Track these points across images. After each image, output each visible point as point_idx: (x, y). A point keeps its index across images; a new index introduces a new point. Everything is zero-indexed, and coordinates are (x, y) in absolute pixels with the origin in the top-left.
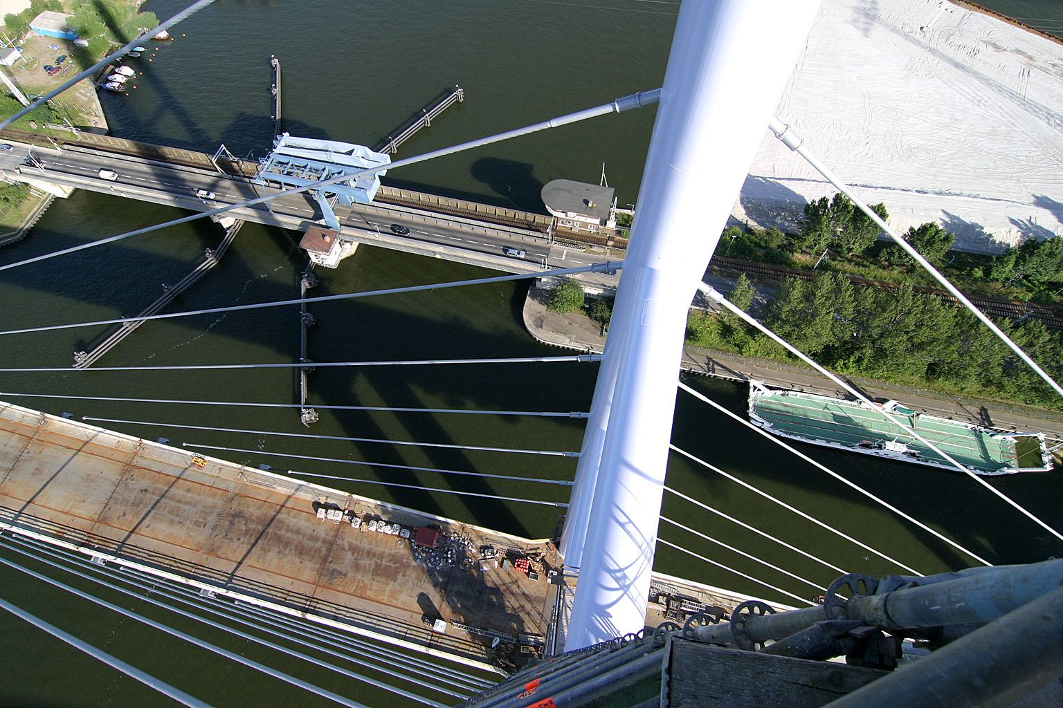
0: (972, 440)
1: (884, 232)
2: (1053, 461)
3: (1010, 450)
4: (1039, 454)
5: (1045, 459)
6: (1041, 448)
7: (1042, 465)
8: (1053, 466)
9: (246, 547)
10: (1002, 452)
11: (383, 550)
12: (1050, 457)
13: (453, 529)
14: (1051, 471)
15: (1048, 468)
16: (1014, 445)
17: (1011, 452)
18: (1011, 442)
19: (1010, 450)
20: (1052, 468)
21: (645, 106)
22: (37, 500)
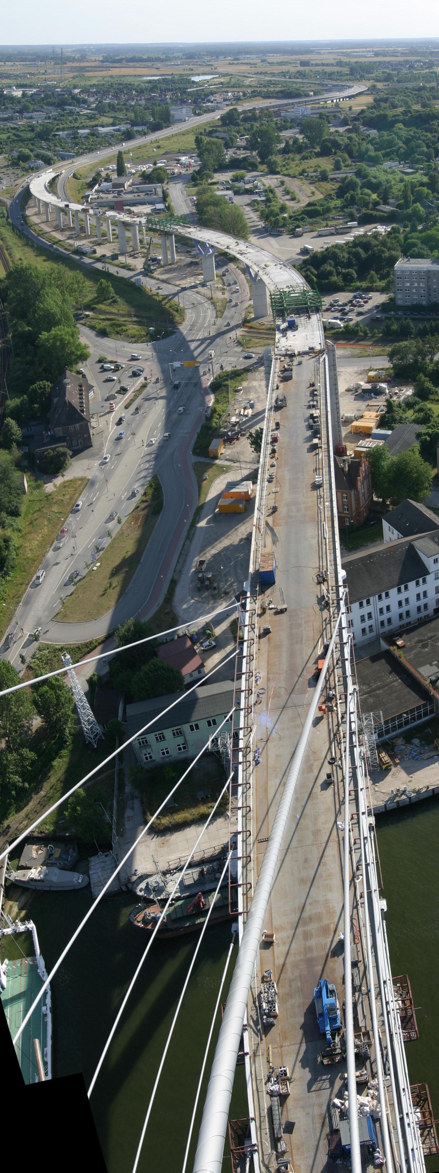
0: (11, 1011)
1: (230, 254)
2: (23, 921)
3: (17, 967)
4: (17, 935)
5: (22, 928)
6: (10, 933)
7: (29, 932)
8: (28, 920)
9: (279, 712)
10: (20, 975)
11: (60, 76)
12: (19, 923)
13: (218, 585)
14: (34, 923)
15: (31, 925)
16: (12, 962)
17: (19, 965)
18: (7, 965)
19: (17, 967)
20: (32, 921)
21: (60, 687)
22: (298, 1046)
